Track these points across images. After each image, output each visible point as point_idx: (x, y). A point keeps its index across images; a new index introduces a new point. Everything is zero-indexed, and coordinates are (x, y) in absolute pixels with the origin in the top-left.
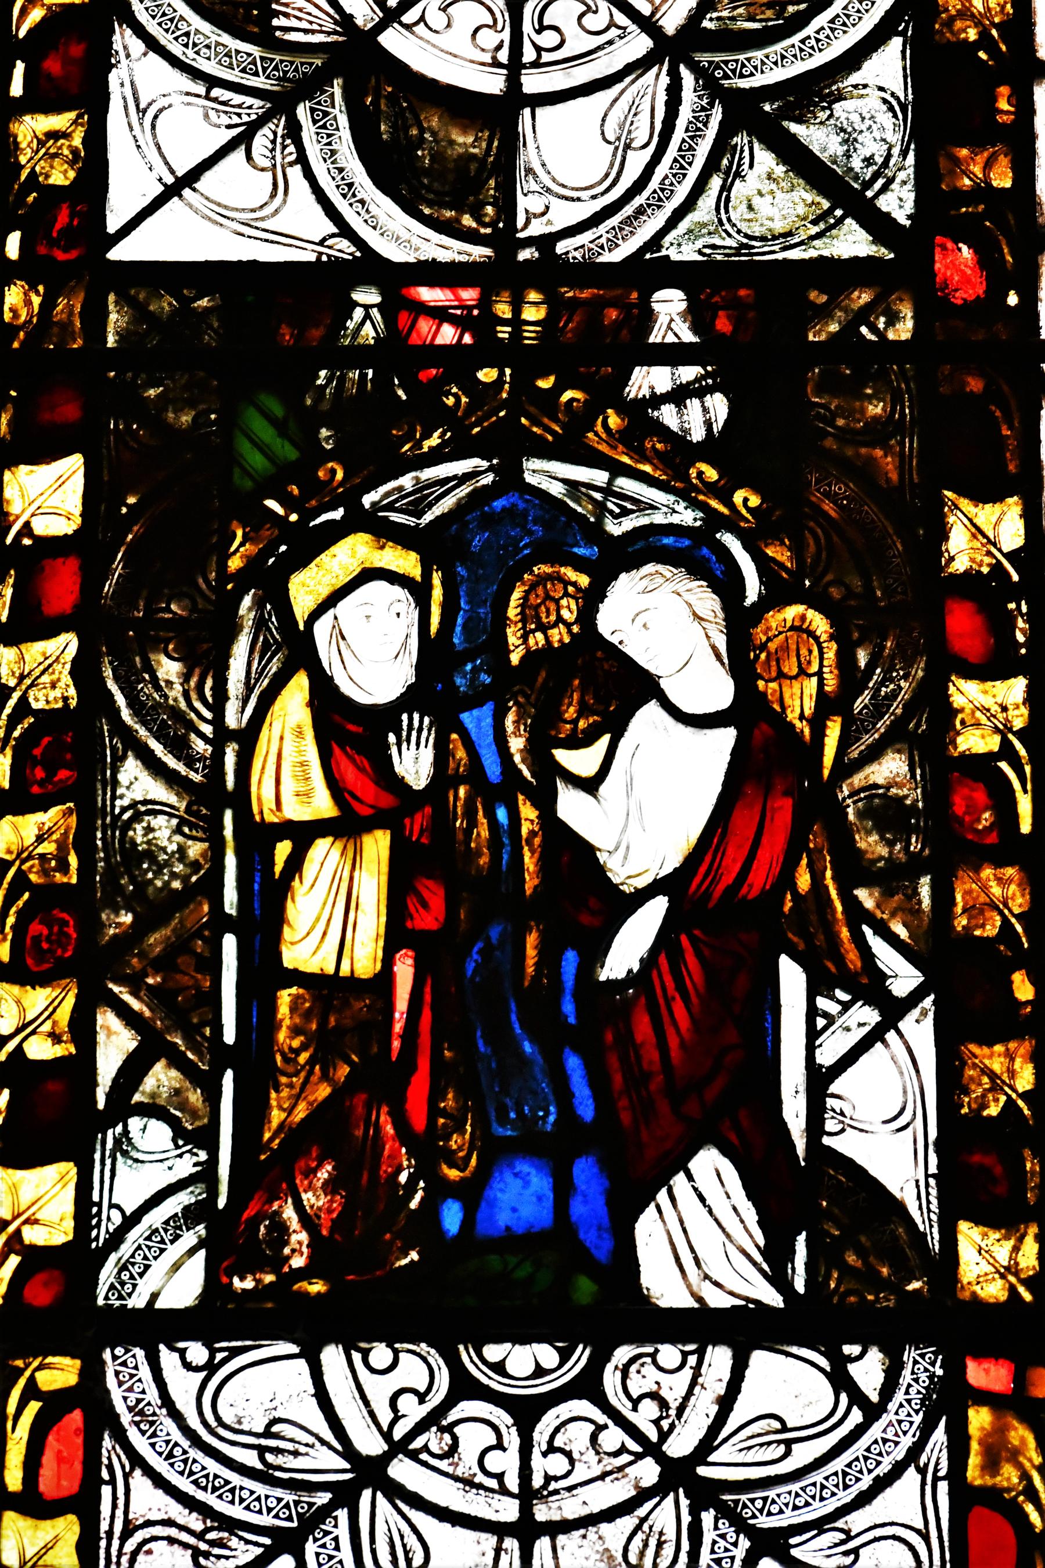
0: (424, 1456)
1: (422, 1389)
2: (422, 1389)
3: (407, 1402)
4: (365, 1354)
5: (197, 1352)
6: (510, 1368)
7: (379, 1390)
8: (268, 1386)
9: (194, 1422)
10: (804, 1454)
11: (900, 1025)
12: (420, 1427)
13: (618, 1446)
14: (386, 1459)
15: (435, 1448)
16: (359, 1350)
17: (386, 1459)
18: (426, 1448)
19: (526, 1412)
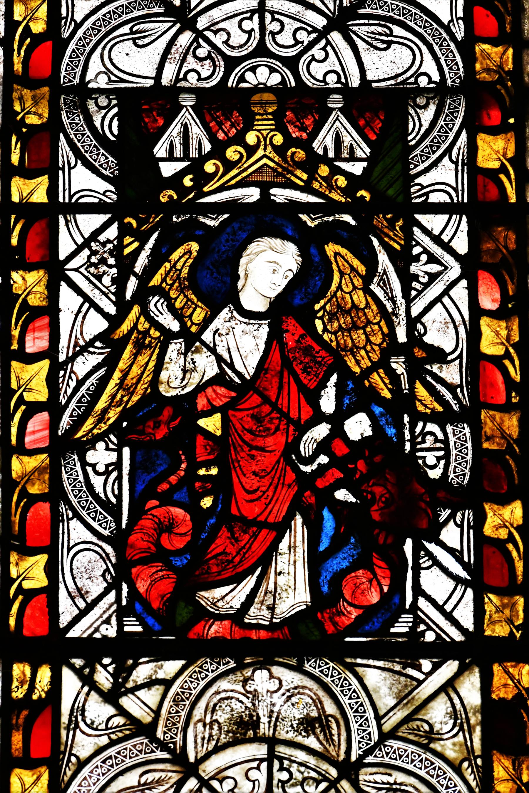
0: (310, 29)
1: (314, 63)
2: (314, 63)
3: (320, 55)
4: (339, 81)
5: (423, 81)
6: (266, 70)
7: (332, 63)
8: (385, 65)
9: (424, 48)
10: (126, 29)
11: (76, 247)
12: (312, 45)
13: (218, 35)
14: (194, 29)
15: (304, 33)
16: (342, 83)
17: (194, 29)
18: (309, 33)
19: (261, 50)
